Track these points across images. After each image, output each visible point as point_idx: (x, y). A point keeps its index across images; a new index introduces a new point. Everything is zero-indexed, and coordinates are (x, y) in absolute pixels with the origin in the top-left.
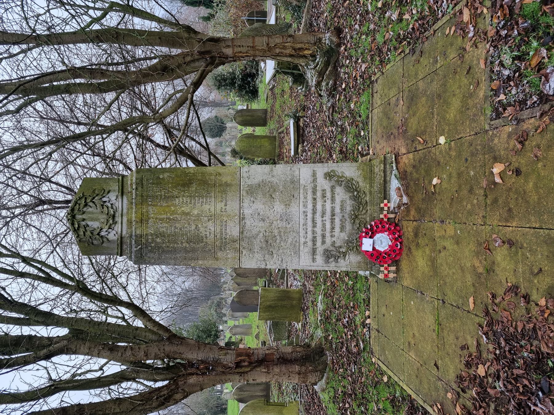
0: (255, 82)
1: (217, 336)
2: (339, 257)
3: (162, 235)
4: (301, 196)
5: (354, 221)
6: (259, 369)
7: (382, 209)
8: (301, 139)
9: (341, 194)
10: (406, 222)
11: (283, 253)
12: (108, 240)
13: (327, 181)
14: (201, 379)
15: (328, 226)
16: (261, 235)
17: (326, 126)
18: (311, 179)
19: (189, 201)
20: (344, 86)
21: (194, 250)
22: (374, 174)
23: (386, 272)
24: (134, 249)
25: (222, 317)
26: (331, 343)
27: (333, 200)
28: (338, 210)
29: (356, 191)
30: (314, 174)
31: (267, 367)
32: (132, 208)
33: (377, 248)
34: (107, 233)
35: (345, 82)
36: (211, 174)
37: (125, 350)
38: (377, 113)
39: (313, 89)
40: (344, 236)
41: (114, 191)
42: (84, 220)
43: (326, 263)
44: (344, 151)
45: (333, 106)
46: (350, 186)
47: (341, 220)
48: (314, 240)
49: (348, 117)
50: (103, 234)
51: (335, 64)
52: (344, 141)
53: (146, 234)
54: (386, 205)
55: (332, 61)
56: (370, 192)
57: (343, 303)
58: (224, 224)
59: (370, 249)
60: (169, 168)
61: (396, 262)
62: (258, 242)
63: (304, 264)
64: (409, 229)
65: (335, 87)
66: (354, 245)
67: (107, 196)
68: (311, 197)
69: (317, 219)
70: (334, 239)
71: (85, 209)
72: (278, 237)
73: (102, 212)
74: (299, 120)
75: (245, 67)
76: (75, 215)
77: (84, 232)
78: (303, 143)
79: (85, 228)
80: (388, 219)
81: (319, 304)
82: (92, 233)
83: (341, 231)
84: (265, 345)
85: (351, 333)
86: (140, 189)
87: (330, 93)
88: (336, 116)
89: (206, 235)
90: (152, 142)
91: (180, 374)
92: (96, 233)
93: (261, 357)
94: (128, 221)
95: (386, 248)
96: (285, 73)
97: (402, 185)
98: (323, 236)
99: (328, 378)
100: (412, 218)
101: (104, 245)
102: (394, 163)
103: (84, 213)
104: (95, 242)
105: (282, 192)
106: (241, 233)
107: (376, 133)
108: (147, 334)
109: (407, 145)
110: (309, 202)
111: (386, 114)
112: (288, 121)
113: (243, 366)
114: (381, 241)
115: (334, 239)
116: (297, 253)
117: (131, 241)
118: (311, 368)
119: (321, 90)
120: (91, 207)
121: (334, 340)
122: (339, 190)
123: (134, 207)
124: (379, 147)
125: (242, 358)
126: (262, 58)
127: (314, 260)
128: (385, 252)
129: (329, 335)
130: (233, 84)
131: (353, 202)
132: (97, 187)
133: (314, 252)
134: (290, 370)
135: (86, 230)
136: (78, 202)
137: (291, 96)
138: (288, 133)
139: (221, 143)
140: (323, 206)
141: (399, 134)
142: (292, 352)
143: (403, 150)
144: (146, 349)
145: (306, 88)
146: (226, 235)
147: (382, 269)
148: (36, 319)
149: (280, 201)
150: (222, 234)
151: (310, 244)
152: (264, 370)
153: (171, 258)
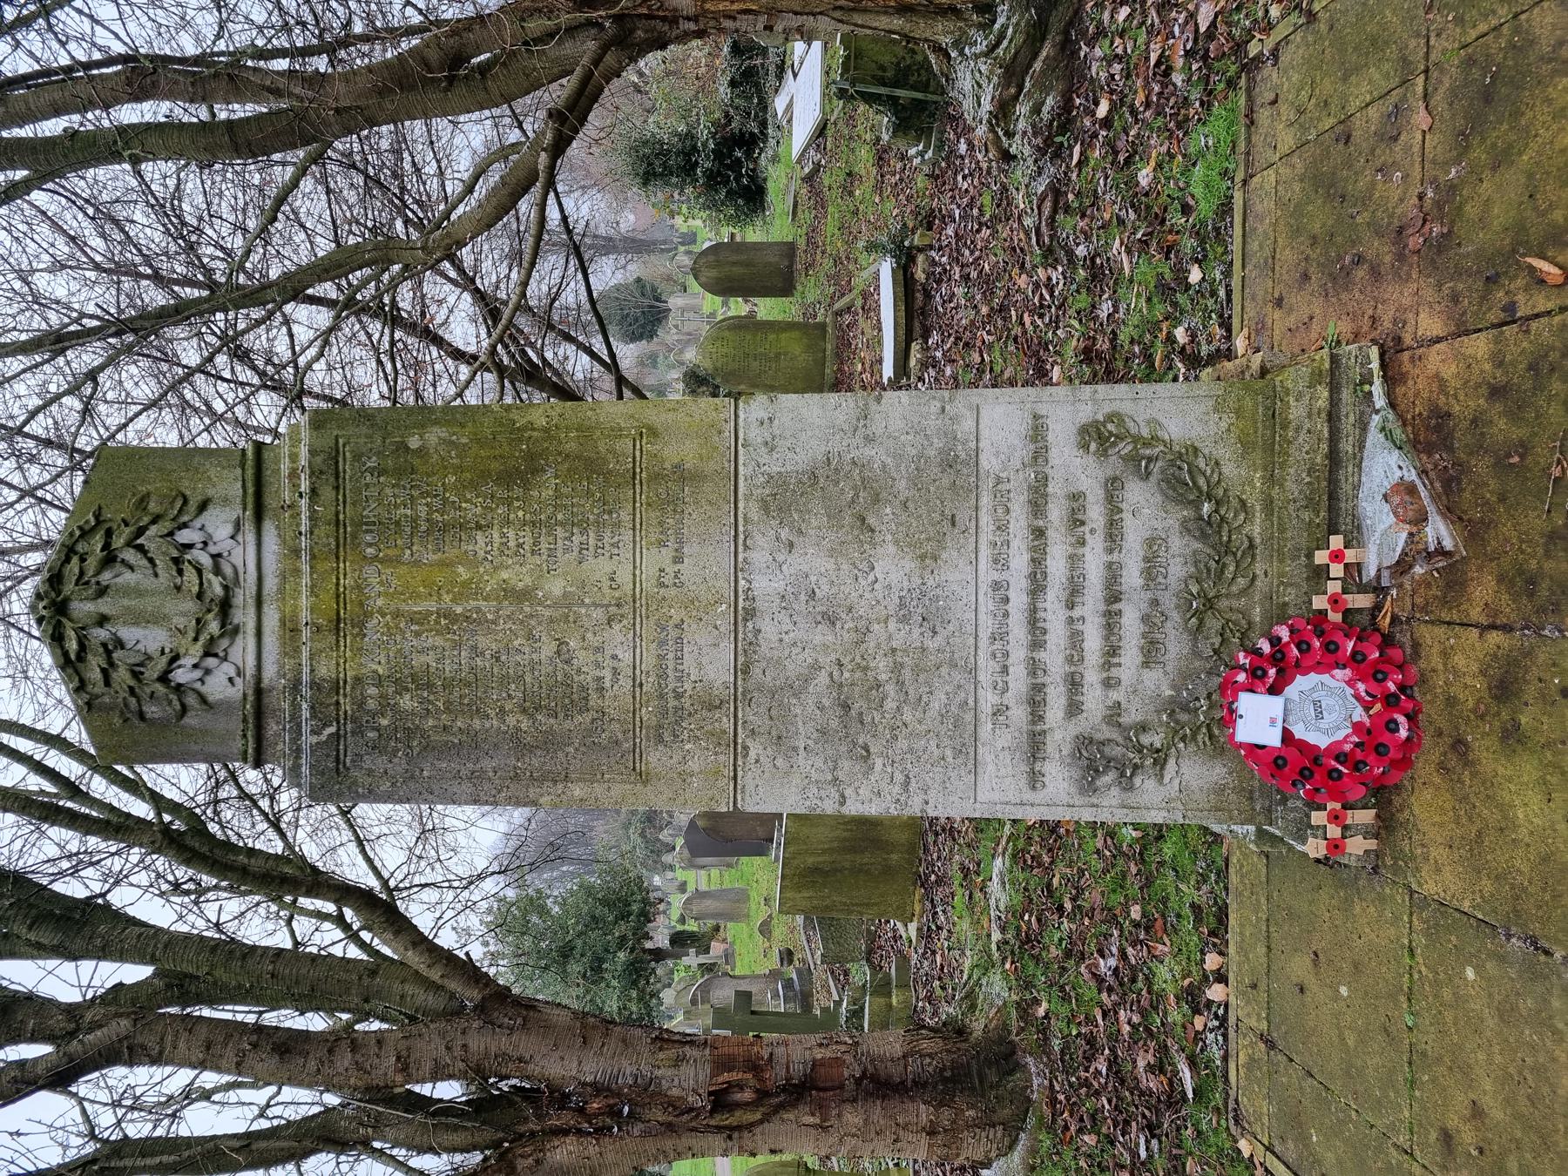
0: (755, 161)
1: (646, 917)
2: (1136, 767)
3: (422, 682)
4: (985, 519)
5: (1201, 621)
6: (791, 1116)
7: (1321, 573)
8: (917, 324)
9: (1145, 508)
10: (1440, 631)
11: (911, 750)
12: (203, 699)
13: (1091, 459)
14: (593, 1150)
15: (1093, 642)
16: (823, 678)
17: (1022, 266)
18: (1023, 452)
19: (529, 541)
20: (1103, 110)
21: (550, 742)
22: (1285, 427)
23: (1334, 831)
24: (308, 740)
25: (659, 853)
26: (1044, 1030)
27: (1113, 535)
28: (1132, 577)
29: (1209, 498)
30: (1037, 432)
31: (821, 1108)
32: (297, 572)
33: (1299, 732)
34: (198, 674)
35: (1112, 92)
36: (617, 432)
37: (330, 1051)
38: (1271, 190)
39: (981, 131)
40: (1158, 682)
41: (226, 501)
42: (102, 620)
43: (1083, 791)
44: (1099, 355)
45: (1056, 191)
46: (1184, 478)
47: (1146, 619)
48: (1036, 701)
49: (1121, 222)
50: (181, 676)
51: (1066, 33)
52: (1103, 315)
53: (358, 680)
54: (1337, 556)
55: (1056, 22)
56: (1268, 505)
57: (1093, 897)
58: (673, 633)
59: (1273, 739)
60: (447, 407)
61: (1382, 795)
62: (811, 707)
63: (996, 796)
64: (1459, 660)
65: (1065, 119)
66: (1203, 720)
67: (197, 523)
68: (1023, 523)
69: (1049, 616)
70: (1115, 695)
71: (106, 577)
72: (890, 689)
73: (178, 588)
74: (912, 259)
75: (727, 115)
76: (66, 601)
77: (104, 671)
78: (926, 336)
79: (108, 653)
80: (1347, 613)
81: (994, 886)
82: (136, 675)
83: (1146, 664)
84: (791, 962)
85: (1136, 1019)
86: (327, 493)
87: (1048, 141)
88: (1069, 225)
89: (600, 679)
90: (438, 341)
91: (522, 1129)
92: (152, 672)
93: (798, 1070)
94: (283, 622)
95: (1340, 736)
96: (869, 99)
97: (1423, 472)
98: (1074, 684)
99: (1033, 1151)
100: (1476, 614)
101: (189, 720)
102: (1377, 382)
103: (102, 591)
104: (151, 710)
105: (905, 505)
106: (743, 670)
107: (1271, 264)
108: (410, 989)
109: (1455, 298)
110: (1015, 544)
111: (1325, 184)
112: (872, 269)
113: (739, 1105)
114: (1317, 705)
115: (1115, 695)
116: (968, 752)
117: (296, 707)
118: (971, 1113)
119: (1010, 135)
120: (132, 568)
121: (1056, 1025)
122: (1140, 497)
123: (305, 568)
124: (1279, 321)
125: (735, 1076)
126: (800, 20)
127: (1035, 779)
128: (1335, 752)
129: (1037, 1002)
130: (688, 169)
131: (1197, 545)
132: (156, 485)
133: (1035, 746)
134: (900, 1120)
135: (112, 664)
136: (80, 548)
137: (878, 188)
138: (870, 306)
139: (653, 358)
140: (1074, 560)
141: (1400, 257)
142: (904, 1057)
143: (1430, 324)
144: (402, 1045)
145: (939, 148)
146: (679, 679)
147: (1318, 818)
148: (32, 936)
149: (896, 543)
150: (663, 676)
151: (1019, 714)
152: (810, 1120)
153: (457, 776)
